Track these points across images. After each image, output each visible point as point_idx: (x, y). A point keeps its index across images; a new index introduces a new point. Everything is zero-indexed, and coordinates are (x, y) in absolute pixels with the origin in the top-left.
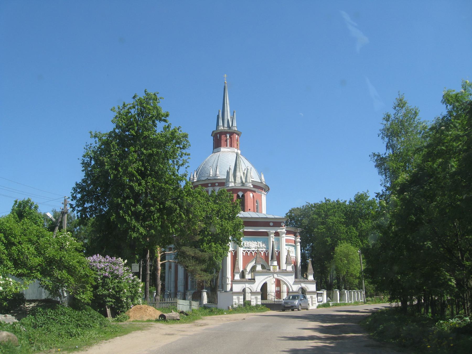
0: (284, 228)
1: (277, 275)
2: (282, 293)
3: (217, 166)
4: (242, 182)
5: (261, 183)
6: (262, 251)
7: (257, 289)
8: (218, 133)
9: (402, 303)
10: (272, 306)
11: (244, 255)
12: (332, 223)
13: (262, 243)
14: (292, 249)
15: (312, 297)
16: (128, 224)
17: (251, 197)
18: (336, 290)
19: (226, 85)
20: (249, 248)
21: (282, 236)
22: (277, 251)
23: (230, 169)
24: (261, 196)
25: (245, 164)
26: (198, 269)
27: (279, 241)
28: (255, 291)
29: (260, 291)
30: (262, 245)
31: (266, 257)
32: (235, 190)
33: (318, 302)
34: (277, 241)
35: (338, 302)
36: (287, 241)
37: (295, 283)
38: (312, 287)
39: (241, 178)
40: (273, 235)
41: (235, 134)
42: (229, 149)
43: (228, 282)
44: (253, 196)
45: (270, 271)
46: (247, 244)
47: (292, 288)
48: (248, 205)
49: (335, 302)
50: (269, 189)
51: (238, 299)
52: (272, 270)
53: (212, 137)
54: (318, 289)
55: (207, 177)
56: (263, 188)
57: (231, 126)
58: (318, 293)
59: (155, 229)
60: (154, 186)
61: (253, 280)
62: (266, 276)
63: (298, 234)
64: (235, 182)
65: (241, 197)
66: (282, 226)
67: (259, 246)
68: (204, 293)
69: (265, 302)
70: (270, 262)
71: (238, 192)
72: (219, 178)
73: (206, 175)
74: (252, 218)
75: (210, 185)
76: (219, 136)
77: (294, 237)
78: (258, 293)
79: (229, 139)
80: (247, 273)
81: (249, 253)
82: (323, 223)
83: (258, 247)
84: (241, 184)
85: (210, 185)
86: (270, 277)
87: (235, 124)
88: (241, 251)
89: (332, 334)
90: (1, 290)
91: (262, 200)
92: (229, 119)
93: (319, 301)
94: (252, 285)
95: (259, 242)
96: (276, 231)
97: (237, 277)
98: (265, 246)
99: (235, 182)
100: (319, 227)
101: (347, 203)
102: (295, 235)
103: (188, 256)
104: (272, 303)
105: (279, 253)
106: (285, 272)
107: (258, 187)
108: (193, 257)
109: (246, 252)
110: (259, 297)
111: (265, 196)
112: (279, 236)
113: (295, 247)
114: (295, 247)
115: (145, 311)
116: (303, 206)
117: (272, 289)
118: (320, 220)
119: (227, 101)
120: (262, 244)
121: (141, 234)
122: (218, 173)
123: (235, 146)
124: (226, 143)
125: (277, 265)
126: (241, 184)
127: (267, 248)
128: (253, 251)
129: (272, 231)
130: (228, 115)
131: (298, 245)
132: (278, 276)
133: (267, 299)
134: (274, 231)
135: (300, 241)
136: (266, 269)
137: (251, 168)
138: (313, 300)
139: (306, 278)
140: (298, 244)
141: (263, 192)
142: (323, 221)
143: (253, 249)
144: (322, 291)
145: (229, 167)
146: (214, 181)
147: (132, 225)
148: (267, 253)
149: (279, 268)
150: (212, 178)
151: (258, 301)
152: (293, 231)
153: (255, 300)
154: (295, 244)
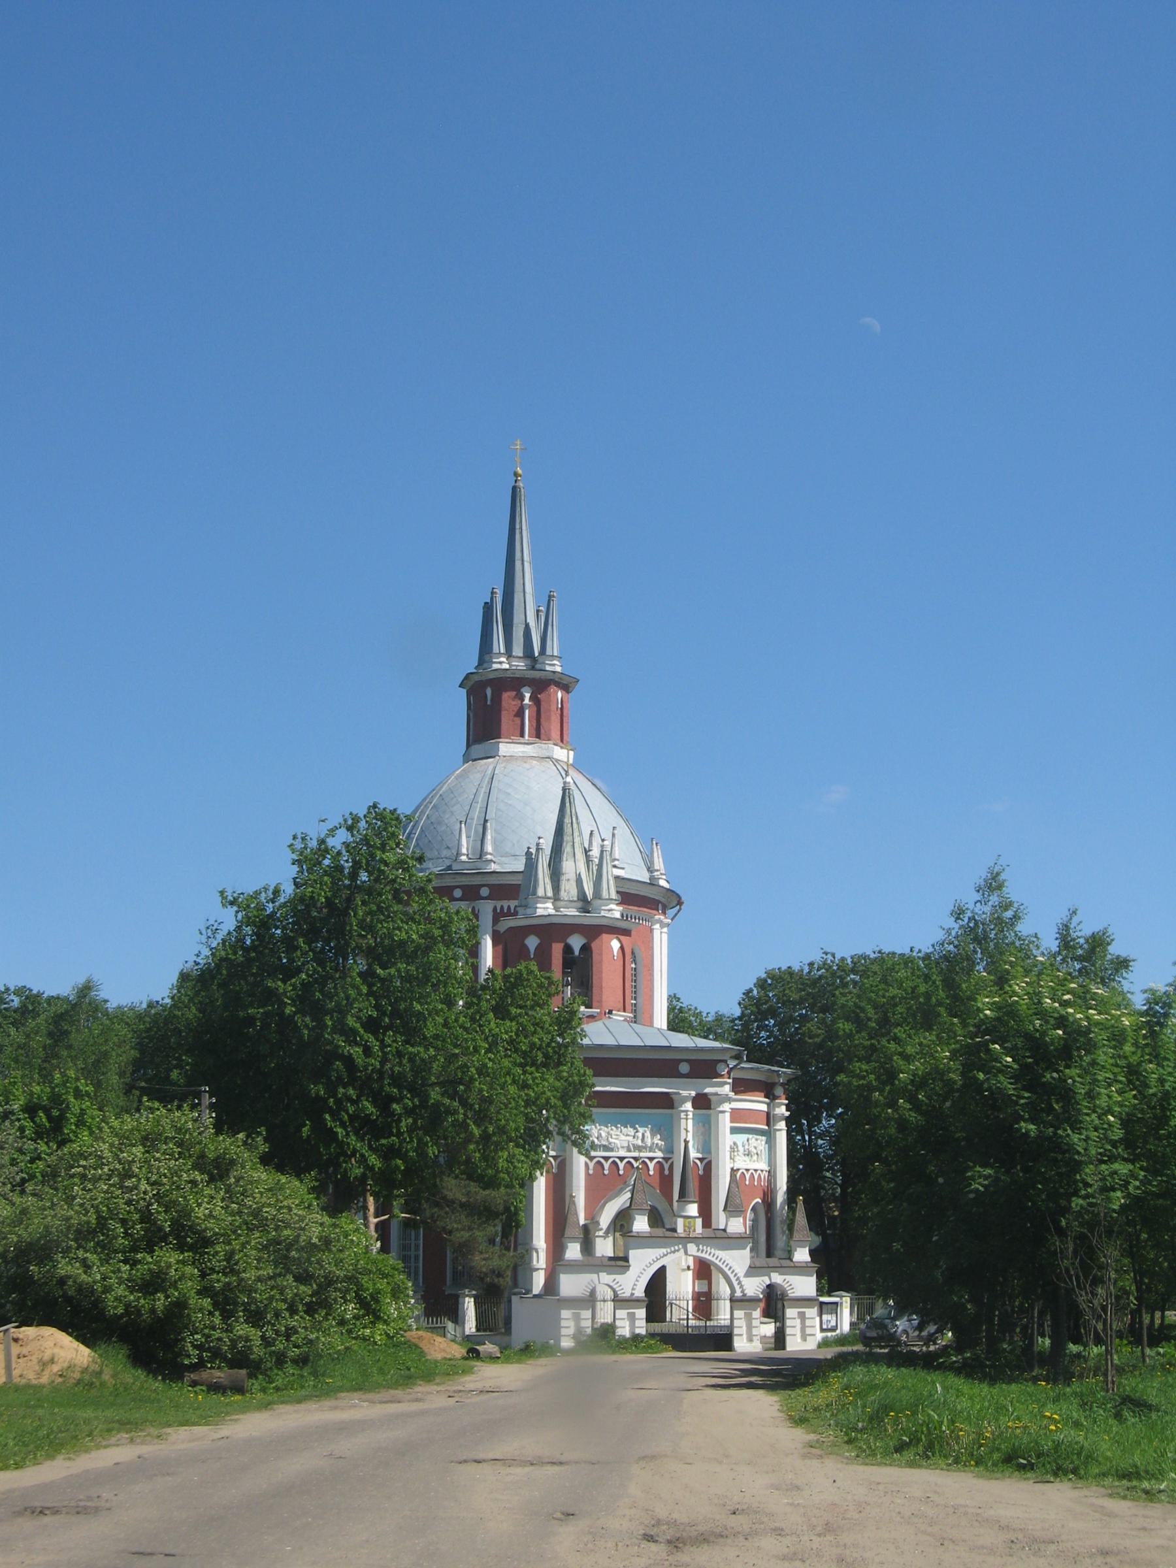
0: (726, 1083)
1: (698, 1246)
2: (714, 1303)
3: (486, 821)
4: (582, 897)
5: (653, 883)
6: (651, 1159)
7: (633, 1289)
9: (1051, 1343)
10: (683, 1341)
11: (591, 1172)
15: (802, 1316)
16: (341, 1144)
17: (615, 954)
20: (606, 1148)
21: (721, 1109)
23: (538, 850)
24: (652, 930)
26: (480, 1240)
28: (627, 1294)
30: (652, 1139)
31: (665, 1180)
32: (552, 931)
33: (822, 1330)
34: (704, 1125)
36: (736, 1115)
37: (753, 1271)
38: (805, 1285)
39: (579, 881)
40: (688, 1106)
41: (553, 688)
42: (530, 746)
43: (535, 1262)
44: (622, 948)
47: (741, 1287)
48: (604, 985)
50: (680, 903)
52: (680, 1229)
53: (464, 692)
54: (820, 1291)
55: (448, 863)
56: (659, 902)
58: (822, 1303)
59: (404, 1157)
60: (399, 1054)
61: (620, 1262)
62: (664, 1251)
63: (779, 1091)
64: (556, 898)
65: (577, 953)
66: (721, 1076)
68: (467, 1299)
69: (657, 1327)
70: (675, 1204)
72: (493, 867)
73: (445, 853)
74: (619, 1047)
75: (458, 893)
77: (767, 1100)
78: (638, 1300)
79: (530, 706)
80: (601, 1233)
81: (607, 1165)
83: (639, 1148)
84: (580, 904)
85: (458, 893)
86: (674, 1252)
87: (554, 648)
88: (580, 1165)
90: (1167, 1367)
91: (652, 948)
92: (531, 620)
93: (825, 1327)
94: (618, 1277)
95: (641, 1130)
97: (573, 1251)
98: (660, 1142)
99: (556, 898)
100: (859, 1066)
102: (770, 1095)
103: (450, 1203)
104: (680, 1331)
105: (708, 1167)
106: (725, 1240)
108: (462, 1205)
109: (599, 1162)
110: (641, 1313)
113: (769, 1135)
114: (769, 1135)
115: (430, 1343)
116: (811, 964)
120: (653, 1135)
121: (372, 1168)
122: (489, 848)
123: (555, 733)
124: (518, 720)
125: (696, 1214)
126: (580, 904)
127: (669, 1150)
128: (622, 1159)
129: (684, 1093)
132: (698, 1250)
133: (664, 1320)
134: (693, 1093)
135: (787, 1114)
136: (663, 1227)
138: (808, 1323)
142: (872, 1045)
143: (622, 1153)
144: (837, 1296)
146: (477, 881)
147: (349, 1148)
148: (666, 1166)
149: (707, 1223)
150: (467, 866)
151: (637, 1325)
153: (627, 1324)
154: (768, 1124)
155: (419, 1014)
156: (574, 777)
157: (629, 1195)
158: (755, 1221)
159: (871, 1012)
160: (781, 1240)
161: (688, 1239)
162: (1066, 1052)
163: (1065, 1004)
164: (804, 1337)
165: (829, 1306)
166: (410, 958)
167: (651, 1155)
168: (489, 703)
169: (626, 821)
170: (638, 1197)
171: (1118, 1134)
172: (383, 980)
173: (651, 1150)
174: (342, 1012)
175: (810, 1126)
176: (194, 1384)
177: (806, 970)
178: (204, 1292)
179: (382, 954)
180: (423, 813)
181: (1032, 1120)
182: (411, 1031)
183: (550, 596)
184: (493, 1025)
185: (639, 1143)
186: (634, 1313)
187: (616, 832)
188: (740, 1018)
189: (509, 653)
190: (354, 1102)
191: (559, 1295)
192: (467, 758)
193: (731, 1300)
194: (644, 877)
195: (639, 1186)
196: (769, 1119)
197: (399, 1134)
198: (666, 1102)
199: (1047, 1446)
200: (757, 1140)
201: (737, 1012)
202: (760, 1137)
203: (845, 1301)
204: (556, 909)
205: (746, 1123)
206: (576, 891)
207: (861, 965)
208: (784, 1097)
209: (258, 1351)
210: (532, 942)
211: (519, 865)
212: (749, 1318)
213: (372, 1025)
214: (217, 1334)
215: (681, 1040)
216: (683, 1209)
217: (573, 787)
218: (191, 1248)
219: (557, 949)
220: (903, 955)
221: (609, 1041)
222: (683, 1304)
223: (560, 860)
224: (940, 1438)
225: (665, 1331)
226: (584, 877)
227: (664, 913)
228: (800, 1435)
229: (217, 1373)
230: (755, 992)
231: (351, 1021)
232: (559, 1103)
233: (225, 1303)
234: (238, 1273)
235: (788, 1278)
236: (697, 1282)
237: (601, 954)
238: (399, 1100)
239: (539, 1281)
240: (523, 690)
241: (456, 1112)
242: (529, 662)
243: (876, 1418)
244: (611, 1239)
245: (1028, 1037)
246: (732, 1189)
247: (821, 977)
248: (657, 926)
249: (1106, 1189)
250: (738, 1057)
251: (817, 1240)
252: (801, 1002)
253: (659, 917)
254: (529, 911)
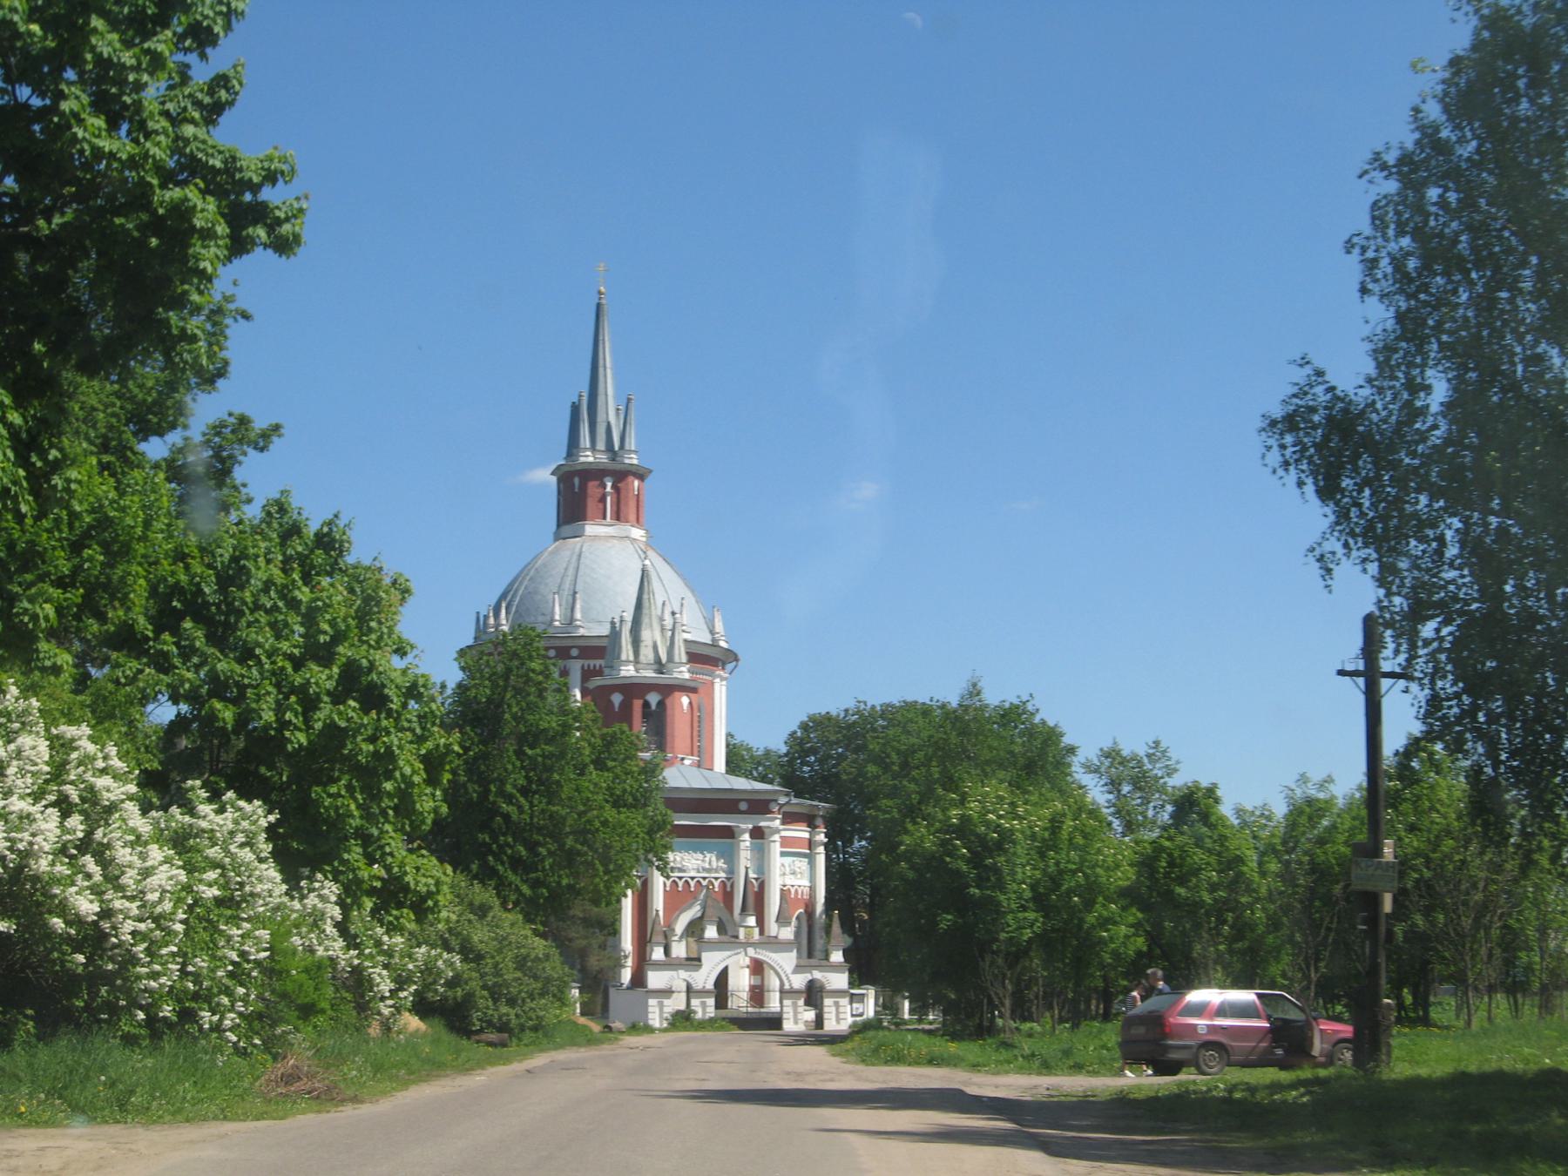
3: (575, 593)
4: (658, 661)
5: (714, 645)
6: (716, 879)
10: (746, 1023)
15: (837, 1005)
20: (681, 870)
22: (756, 879)
23: (621, 621)
24: (713, 683)
25: (669, 589)
27: (761, 855)
31: (728, 896)
32: (633, 690)
33: (853, 1015)
36: (785, 842)
37: (799, 969)
38: (839, 980)
40: (747, 836)
44: (691, 703)
50: (736, 659)
54: (852, 984)
57: (616, 448)
61: (694, 962)
62: (729, 953)
63: (819, 821)
64: (637, 661)
65: (654, 707)
69: (723, 1013)
71: (645, 694)
72: (582, 632)
78: (708, 992)
80: (676, 938)
81: (681, 883)
83: (705, 870)
84: (655, 667)
87: (631, 443)
88: (659, 883)
95: (708, 855)
99: (637, 661)
100: (885, 803)
102: (812, 825)
105: (762, 886)
107: (706, 658)
110: (711, 1002)
113: (811, 858)
114: (811, 858)
116: (846, 711)
117: (741, 981)
120: (718, 860)
122: (578, 615)
123: (632, 517)
124: (601, 505)
126: (655, 667)
128: (693, 878)
129: (743, 826)
130: (610, 411)
134: (750, 826)
138: (841, 1009)
139: (827, 957)
143: (693, 874)
148: (729, 884)
149: (762, 932)
155: (558, 783)
156: (655, 562)
157: (698, 908)
158: (798, 928)
159: (894, 756)
160: (819, 943)
161: (748, 944)
162: (999, 847)
163: (1000, 817)
164: (838, 1020)
166: (550, 741)
167: (716, 875)
169: (693, 591)
170: (709, 912)
171: (1028, 894)
172: (530, 757)
173: (716, 871)
174: (502, 782)
175: (844, 846)
176: (478, 1042)
177: (842, 715)
178: (484, 987)
179: (533, 737)
180: (521, 583)
181: (978, 887)
182: (552, 794)
184: (594, 776)
185: (707, 866)
188: (786, 755)
189: (593, 448)
190: (511, 847)
192: (558, 537)
194: (707, 639)
195: (710, 902)
196: (811, 844)
197: (544, 870)
198: (729, 833)
199: (946, 1056)
201: (784, 749)
203: (870, 993)
204: (637, 670)
207: (888, 712)
209: (514, 1022)
210: (617, 699)
211: (605, 630)
212: (795, 1006)
213: (525, 791)
214: (490, 1012)
215: (741, 783)
216: (744, 921)
217: (650, 568)
218: (472, 961)
219: (637, 704)
220: (924, 704)
221: (683, 784)
222: (740, 994)
224: (904, 1056)
225: (729, 1015)
226: (659, 643)
227: (723, 669)
228: (838, 1059)
229: (492, 1036)
230: (799, 734)
231: (509, 788)
232: (647, 837)
233: (495, 994)
234: (501, 975)
238: (542, 845)
239: (626, 975)
241: (586, 854)
242: (610, 455)
243: (876, 1051)
244: (684, 943)
245: (978, 836)
247: (854, 722)
249: (1020, 928)
250: (787, 795)
251: (848, 941)
252: (837, 743)
253: (720, 672)
254: (614, 672)
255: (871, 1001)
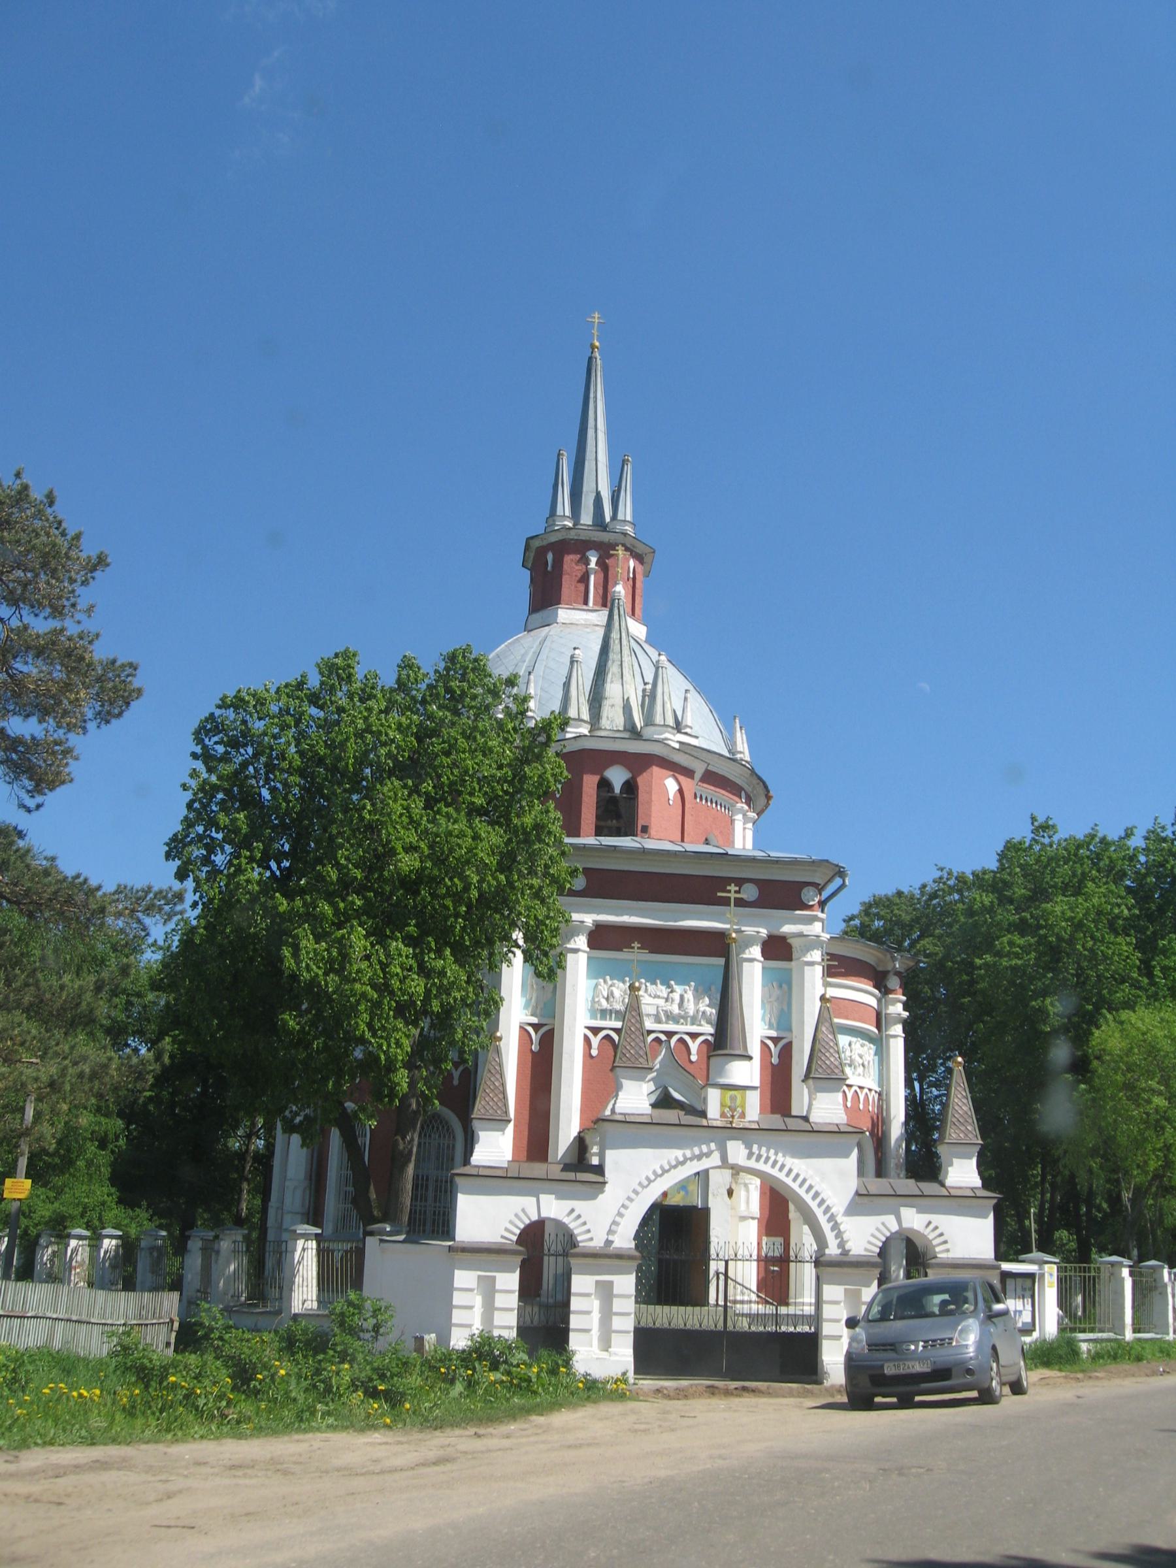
0: (816, 919)
1: (749, 1146)
6: (693, 1036)
7: (610, 1232)
8: (551, 546)
11: (594, 1052)
12: (1066, 920)
13: (696, 990)
14: (862, 1051)
15: (606, 1293)
18: (1115, 1258)
19: (597, 354)
21: (808, 958)
24: (732, 822)
28: (598, 1243)
29: (632, 1245)
34: (780, 986)
35: (1129, 1335)
37: (863, 1202)
40: (756, 951)
42: (594, 614)
44: (681, 791)
45: (704, 1122)
46: (612, 993)
47: (839, 1235)
49: (1111, 1335)
51: (489, 1290)
52: (714, 1111)
56: (741, 789)
57: (608, 519)
58: (1006, 1275)
62: (678, 1154)
63: (894, 982)
65: (617, 790)
66: (810, 908)
67: (681, 1005)
68: (300, 1243)
76: (554, 560)
77: (876, 992)
78: (619, 1256)
82: (1022, 928)
83: (670, 1017)
86: (699, 1157)
87: (626, 511)
89: (654, 919)
94: (580, 1206)
95: (679, 989)
96: (775, 933)
98: (708, 1010)
101: (1137, 842)
102: (879, 980)
110: (509, 1281)
111: (750, 825)
112: (789, 958)
113: (880, 1043)
114: (880, 1043)
118: (1008, 915)
119: (596, 420)
120: (698, 998)
124: (582, 587)
129: (749, 930)
130: (600, 479)
131: (895, 1036)
133: (702, 1301)
134: (764, 932)
135: (906, 1014)
137: (687, 691)
140: (892, 1032)
141: (739, 805)
144: (1032, 1262)
145: (572, 652)
152: (872, 963)
154: (878, 1026)
161: (731, 1130)
165: (1019, 1281)
167: (694, 1029)
168: (549, 568)
173: (694, 1021)
183: (624, 461)
185: (675, 1009)
186: (611, 1283)
187: (688, 695)
191: (453, 1239)
193: (818, 1263)
200: (862, 1046)
202: (867, 1043)
205: (847, 1018)
206: (622, 719)
208: (900, 991)
219: (590, 783)
223: (604, 681)
235: (937, 1219)
236: (765, 1239)
237: (650, 793)
240: (588, 554)
246: (820, 1036)
248: (739, 817)
255: (1050, 1294)
